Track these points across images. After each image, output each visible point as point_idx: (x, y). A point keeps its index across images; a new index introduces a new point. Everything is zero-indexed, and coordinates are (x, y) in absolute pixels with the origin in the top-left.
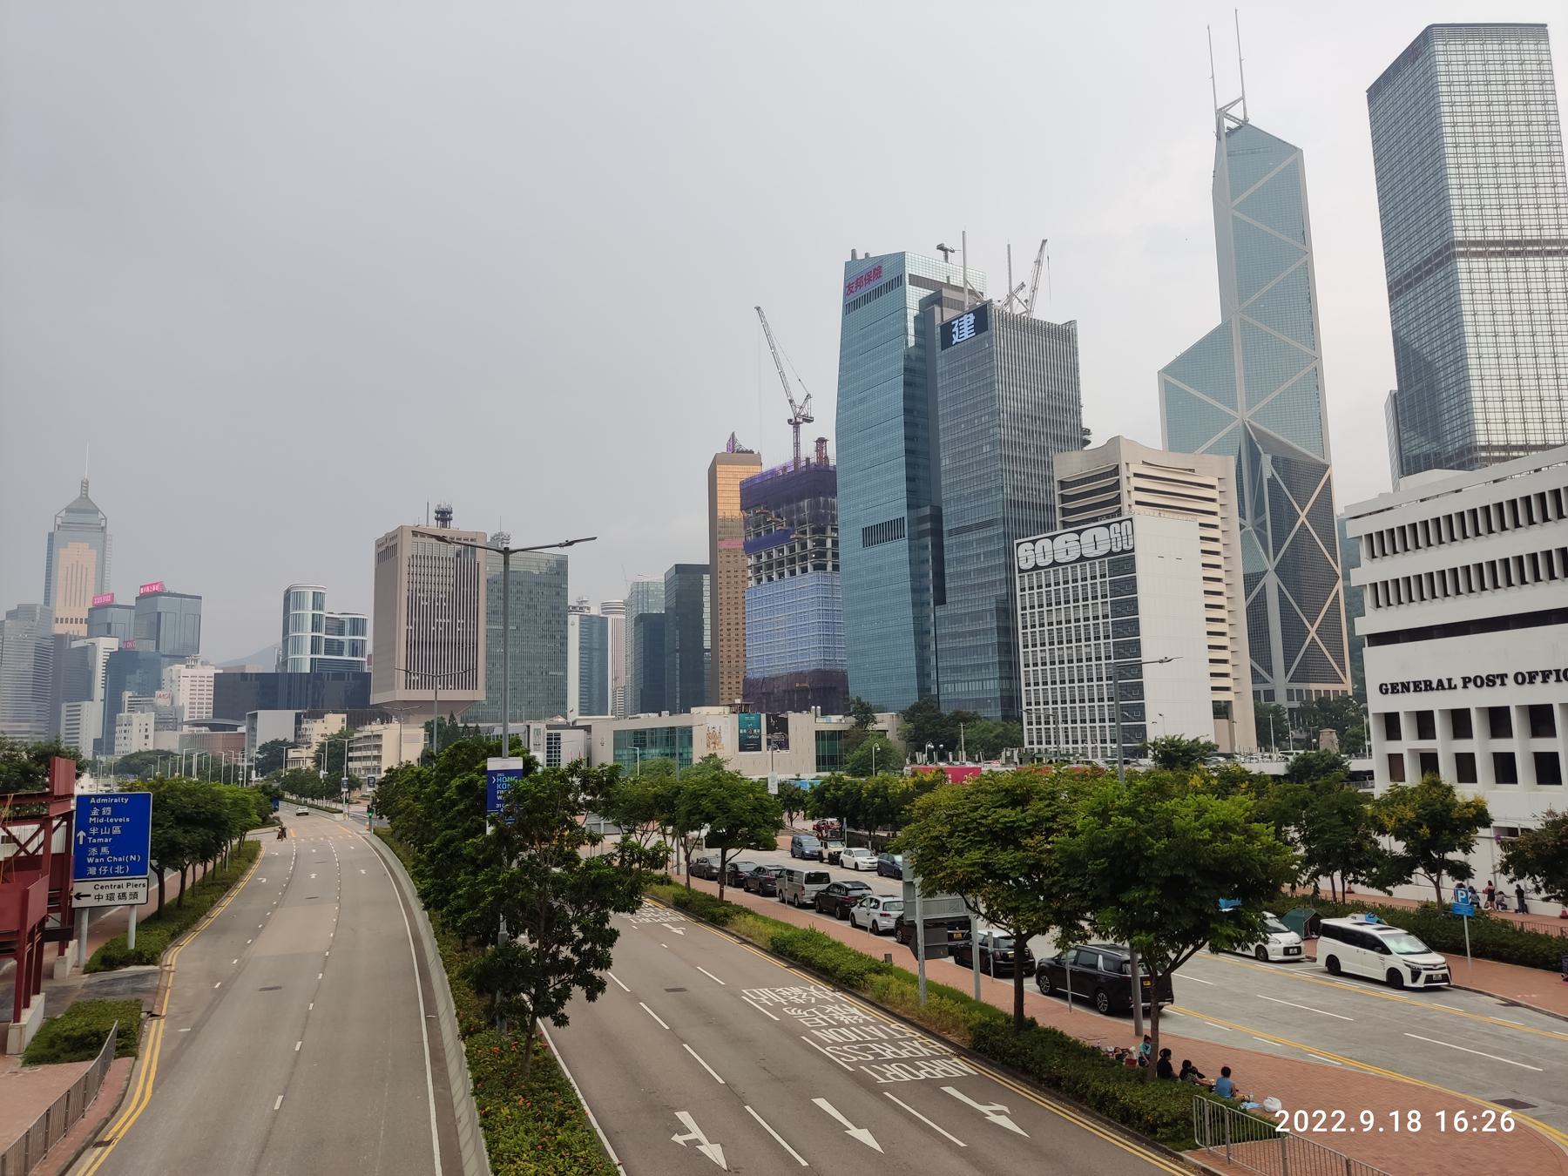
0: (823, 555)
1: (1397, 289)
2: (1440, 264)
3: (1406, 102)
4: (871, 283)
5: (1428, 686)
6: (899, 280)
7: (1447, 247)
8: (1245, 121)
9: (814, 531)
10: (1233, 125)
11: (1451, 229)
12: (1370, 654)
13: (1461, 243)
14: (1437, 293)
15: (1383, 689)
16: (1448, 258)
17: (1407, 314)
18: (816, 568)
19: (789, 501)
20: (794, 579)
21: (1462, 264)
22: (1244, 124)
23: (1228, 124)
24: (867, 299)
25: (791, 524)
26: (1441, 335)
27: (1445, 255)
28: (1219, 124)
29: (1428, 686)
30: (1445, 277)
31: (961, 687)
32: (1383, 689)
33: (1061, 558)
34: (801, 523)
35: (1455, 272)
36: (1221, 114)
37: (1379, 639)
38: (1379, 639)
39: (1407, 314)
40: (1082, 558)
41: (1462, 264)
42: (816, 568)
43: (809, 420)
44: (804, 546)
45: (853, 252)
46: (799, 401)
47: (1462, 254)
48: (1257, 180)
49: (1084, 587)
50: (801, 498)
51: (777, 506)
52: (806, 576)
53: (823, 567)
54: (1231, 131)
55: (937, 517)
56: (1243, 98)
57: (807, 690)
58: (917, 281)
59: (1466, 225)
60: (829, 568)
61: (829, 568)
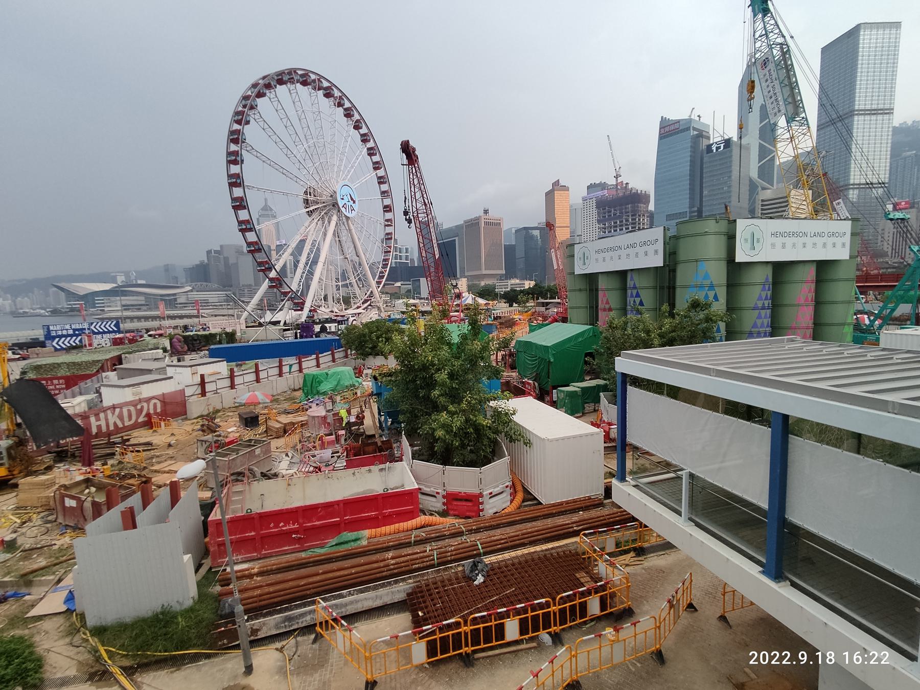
4: (670, 131)
6: (688, 129)
11: (854, 105)
19: (621, 205)
21: (856, 118)
44: (627, 220)
51: (615, 207)
58: (694, 129)
59: (859, 104)
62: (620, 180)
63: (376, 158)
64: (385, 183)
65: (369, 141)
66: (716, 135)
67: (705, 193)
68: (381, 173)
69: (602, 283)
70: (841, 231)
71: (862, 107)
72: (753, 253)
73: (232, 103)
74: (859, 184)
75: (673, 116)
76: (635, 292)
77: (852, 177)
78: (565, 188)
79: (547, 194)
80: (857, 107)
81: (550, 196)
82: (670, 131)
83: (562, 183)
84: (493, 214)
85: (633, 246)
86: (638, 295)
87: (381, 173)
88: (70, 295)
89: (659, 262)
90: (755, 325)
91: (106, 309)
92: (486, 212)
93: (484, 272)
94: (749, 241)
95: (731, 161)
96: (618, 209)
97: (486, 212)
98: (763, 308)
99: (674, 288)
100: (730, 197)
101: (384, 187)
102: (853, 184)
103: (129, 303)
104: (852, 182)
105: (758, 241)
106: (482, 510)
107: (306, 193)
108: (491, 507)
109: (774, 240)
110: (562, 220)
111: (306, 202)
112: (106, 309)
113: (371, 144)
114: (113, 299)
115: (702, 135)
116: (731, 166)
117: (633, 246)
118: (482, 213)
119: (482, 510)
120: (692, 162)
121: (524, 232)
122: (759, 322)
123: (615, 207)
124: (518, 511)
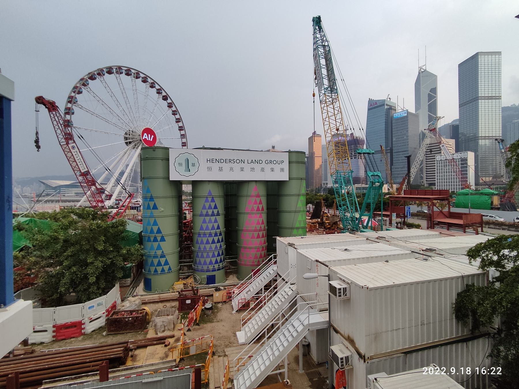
4: (374, 106)
6: (384, 105)
11: (478, 94)
21: (480, 101)
22: (425, 70)
23: (422, 70)
24: (375, 108)
34: (351, 150)
44: (351, 154)
54: (422, 72)
55: (391, 150)
58: (387, 105)
59: (481, 93)
63: (178, 116)
64: (183, 130)
65: (172, 107)
66: (399, 108)
67: (394, 139)
68: (180, 124)
70: (279, 159)
71: (483, 95)
72: (187, 174)
73: (74, 81)
74: (485, 137)
75: (377, 97)
77: (480, 133)
79: (309, 139)
80: (480, 95)
82: (374, 106)
87: (180, 124)
88: (48, 186)
90: (202, 228)
91: (66, 195)
92: (273, 147)
94: (184, 165)
95: (407, 123)
96: (347, 146)
100: (408, 142)
101: (183, 132)
102: (481, 137)
103: (79, 192)
104: (480, 135)
105: (193, 165)
106: (84, 329)
107: (126, 134)
108: (89, 328)
109: (210, 164)
110: (318, 152)
111: (126, 138)
112: (66, 195)
113: (174, 109)
114: (70, 189)
115: (391, 108)
116: (407, 126)
119: (84, 329)
120: (386, 123)
122: (205, 226)
124: (422, 252)
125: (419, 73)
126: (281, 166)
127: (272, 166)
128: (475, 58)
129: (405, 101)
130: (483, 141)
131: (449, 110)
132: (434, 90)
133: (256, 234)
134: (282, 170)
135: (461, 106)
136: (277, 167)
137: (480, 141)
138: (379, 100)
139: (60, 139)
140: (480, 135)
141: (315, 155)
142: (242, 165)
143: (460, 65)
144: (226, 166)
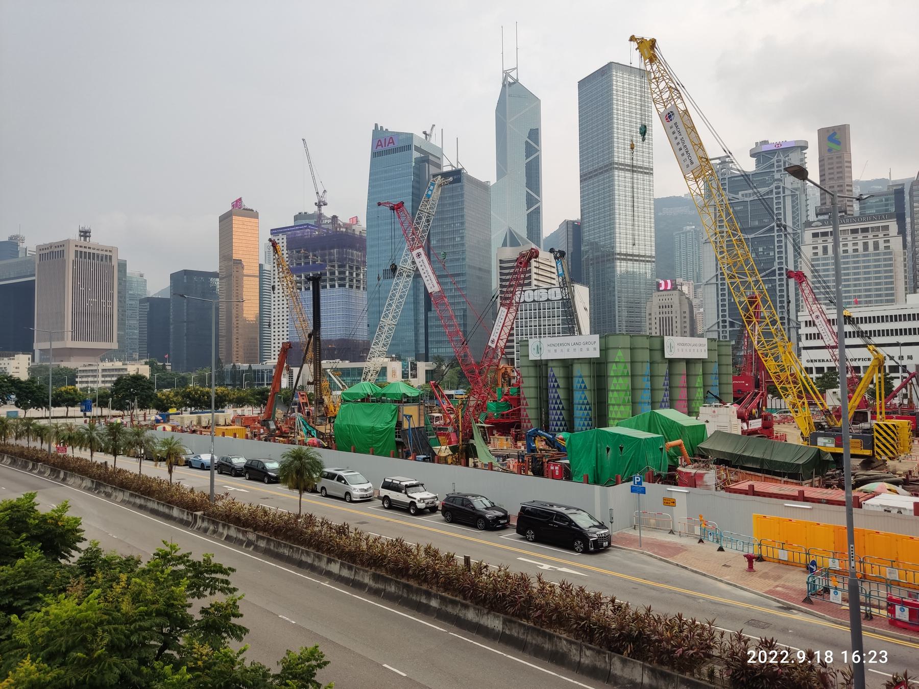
0: (344, 279)
1: (585, 178)
2: (606, 171)
3: (596, 90)
4: (388, 147)
5: (823, 361)
6: (409, 147)
7: (611, 164)
8: (517, 80)
9: (339, 267)
10: (511, 81)
11: (613, 156)
12: (803, 352)
13: (617, 164)
14: (604, 184)
15: (808, 361)
16: (611, 169)
17: (588, 190)
18: (340, 286)
19: (323, 249)
20: (332, 290)
21: (616, 172)
22: (516, 81)
24: (388, 152)
25: (324, 261)
26: (604, 203)
27: (609, 167)
28: (505, 79)
29: (823, 361)
30: (609, 177)
31: (440, 350)
32: (808, 361)
33: (527, 300)
34: (331, 261)
35: (613, 176)
36: (506, 74)
37: (805, 348)
38: (805, 348)
39: (588, 190)
40: (548, 300)
41: (616, 172)
42: (340, 286)
43: (325, 204)
44: (333, 273)
45: (376, 125)
46: (321, 194)
47: (617, 168)
48: (516, 109)
49: (539, 313)
50: (333, 248)
51: (314, 250)
52: (334, 290)
53: (344, 286)
54: (510, 84)
56: (517, 68)
57: (335, 349)
58: (418, 149)
60: (347, 286)
61: (347, 286)
62: (324, 210)
69: (578, 370)
70: (592, 341)
74: (626, 255)
75: (393, 126)
76: (581, 380)
78: (252, 214)
81: (226, 221)
82: (388, 147)
83: (247, 204)
84: (98, 239)
85: (696, 345)
86: (556, 381)
89: (596, 354)
93: (70, 344)
95: (462, 202)
97: (85, 234)
98: (614, 405)
99: (572, 378)
100: (463, 252)
102: (619, 254)
117: (696, 345)
118: (74, 235)
121: (187, 282)
123: (314, 250)
125: (504, 85)
126: (594, 346)
127: (587, 346)
128: (605, 72)
129: (473, 152)
130: (624, 264)
131: (562, 202)
132: (534, 134)
133: (583, 407)
134: (595, 349)
135: (584, 178)
136: (591, 347)
137: (618, 263)
138: (398, 134)
139: (503, 333)
140: (618, 250)
141: (245, 272)
142: (568, 347)
143: (582, 84)
144: (559, 348)
